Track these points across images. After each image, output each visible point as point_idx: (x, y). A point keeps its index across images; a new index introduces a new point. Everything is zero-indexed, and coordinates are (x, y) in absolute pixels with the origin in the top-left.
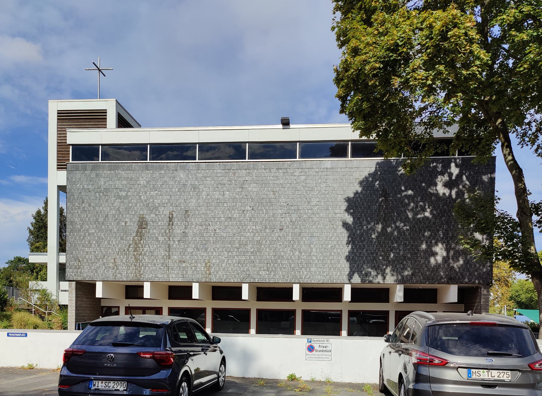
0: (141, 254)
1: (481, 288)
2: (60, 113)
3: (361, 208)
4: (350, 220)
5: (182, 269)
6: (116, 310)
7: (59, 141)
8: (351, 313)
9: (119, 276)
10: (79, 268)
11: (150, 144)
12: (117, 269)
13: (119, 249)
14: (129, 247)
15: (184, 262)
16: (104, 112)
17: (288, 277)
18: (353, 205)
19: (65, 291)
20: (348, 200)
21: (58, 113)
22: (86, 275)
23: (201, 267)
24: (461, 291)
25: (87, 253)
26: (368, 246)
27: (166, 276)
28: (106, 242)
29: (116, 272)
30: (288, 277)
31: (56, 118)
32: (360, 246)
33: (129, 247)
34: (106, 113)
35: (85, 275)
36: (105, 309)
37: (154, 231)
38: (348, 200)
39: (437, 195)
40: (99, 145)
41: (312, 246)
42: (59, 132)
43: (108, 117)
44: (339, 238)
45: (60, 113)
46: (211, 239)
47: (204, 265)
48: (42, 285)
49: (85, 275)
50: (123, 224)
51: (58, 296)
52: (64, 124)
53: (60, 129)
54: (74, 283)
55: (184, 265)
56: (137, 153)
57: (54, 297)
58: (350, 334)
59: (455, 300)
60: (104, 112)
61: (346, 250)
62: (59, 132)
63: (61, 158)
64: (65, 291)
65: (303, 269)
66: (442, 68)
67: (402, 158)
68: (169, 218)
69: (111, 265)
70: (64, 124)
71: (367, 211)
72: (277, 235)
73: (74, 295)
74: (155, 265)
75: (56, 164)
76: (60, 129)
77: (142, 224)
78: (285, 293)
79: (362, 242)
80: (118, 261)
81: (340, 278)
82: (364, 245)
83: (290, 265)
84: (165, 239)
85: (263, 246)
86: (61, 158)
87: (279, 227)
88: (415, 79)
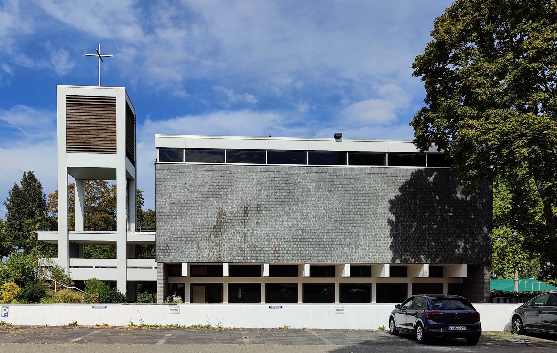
0: (221, 240)
1: (483, 266)
2: (68, 98)
3: (396, 204)
4: (393, 218)
5: (256, 252)
6: (182, 286)
7: (69, 125)
8: (268, 286)
9: (202, 258)
10: (167, 252)
11: (227, 150)
12: (201, 253)
13: (202, 236)
14: (211, 234)
15: (257, 246)
16: (114, 99)
17: (341, 258)
18: (394, 205)
19: (74, 267)
20: (391, 202)
21: (67, 98)
22: (171, 258)
23: (271, 250)
24: (430, 268)
25: (174, 238)
26: (402, 235)
27: (242, 258)
28: (190, 230)
29: (199, 255)
30: (341, 258)
31: (65, 102)
32: (396, 234)
33: (211, 234)
34: (115, 100)
35: (172, 257)
36: (171, 286)
37: (234, 220)
38: (391, 202)
39: (457, 199)
40: (183, 149)
41: (360, 234)
42: (68, 116)
43: (117, 104)
44: (381, 228)
45: (68, 98)
46: (279, 228)
47: (274, 249)
48: (55, 262)
49: (172, 257)
50: (205, 215)
51: (69, 272)
52: (73, 108)
53: (69, 113)
54: (162, 264)
55: (257, 249)
56: (217, 156)
57: (66, 274)
58: (378, 301)
59: (427, 275)
60: (114, 99)
61: (390, 241)
62: (68, 116)
63: (70, 141)
64: (74, 267)
65: (353, 252)
66: (536, 148)
67: (426, 167)
68: (244, 210)
69: (195, 249)
70: (73, 108)
71: (401, 208)
72: (332, 225)
73: (162, 275)
74: (233, 249)
75: (66, 146)
76: (69, 113)
77: (222, 215)
78: (256, 270)
79: (397, 231)
80: (202, 246)
81: (382, 259)
82: (399, 234)
83: (343, 249)
84: (241, 228)
85: (321, 234)
86: (70, 141)
87: (334, 219)
88: (520, 152)
